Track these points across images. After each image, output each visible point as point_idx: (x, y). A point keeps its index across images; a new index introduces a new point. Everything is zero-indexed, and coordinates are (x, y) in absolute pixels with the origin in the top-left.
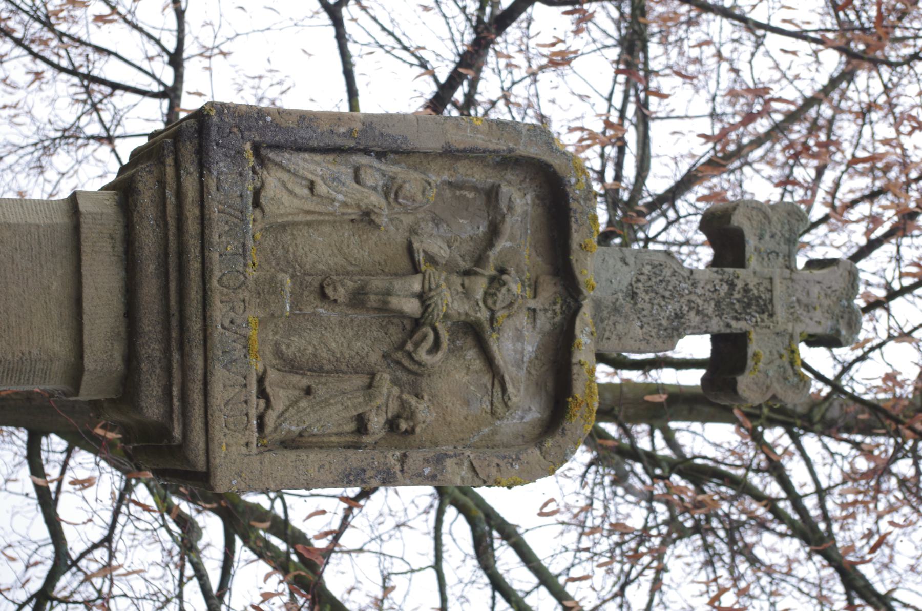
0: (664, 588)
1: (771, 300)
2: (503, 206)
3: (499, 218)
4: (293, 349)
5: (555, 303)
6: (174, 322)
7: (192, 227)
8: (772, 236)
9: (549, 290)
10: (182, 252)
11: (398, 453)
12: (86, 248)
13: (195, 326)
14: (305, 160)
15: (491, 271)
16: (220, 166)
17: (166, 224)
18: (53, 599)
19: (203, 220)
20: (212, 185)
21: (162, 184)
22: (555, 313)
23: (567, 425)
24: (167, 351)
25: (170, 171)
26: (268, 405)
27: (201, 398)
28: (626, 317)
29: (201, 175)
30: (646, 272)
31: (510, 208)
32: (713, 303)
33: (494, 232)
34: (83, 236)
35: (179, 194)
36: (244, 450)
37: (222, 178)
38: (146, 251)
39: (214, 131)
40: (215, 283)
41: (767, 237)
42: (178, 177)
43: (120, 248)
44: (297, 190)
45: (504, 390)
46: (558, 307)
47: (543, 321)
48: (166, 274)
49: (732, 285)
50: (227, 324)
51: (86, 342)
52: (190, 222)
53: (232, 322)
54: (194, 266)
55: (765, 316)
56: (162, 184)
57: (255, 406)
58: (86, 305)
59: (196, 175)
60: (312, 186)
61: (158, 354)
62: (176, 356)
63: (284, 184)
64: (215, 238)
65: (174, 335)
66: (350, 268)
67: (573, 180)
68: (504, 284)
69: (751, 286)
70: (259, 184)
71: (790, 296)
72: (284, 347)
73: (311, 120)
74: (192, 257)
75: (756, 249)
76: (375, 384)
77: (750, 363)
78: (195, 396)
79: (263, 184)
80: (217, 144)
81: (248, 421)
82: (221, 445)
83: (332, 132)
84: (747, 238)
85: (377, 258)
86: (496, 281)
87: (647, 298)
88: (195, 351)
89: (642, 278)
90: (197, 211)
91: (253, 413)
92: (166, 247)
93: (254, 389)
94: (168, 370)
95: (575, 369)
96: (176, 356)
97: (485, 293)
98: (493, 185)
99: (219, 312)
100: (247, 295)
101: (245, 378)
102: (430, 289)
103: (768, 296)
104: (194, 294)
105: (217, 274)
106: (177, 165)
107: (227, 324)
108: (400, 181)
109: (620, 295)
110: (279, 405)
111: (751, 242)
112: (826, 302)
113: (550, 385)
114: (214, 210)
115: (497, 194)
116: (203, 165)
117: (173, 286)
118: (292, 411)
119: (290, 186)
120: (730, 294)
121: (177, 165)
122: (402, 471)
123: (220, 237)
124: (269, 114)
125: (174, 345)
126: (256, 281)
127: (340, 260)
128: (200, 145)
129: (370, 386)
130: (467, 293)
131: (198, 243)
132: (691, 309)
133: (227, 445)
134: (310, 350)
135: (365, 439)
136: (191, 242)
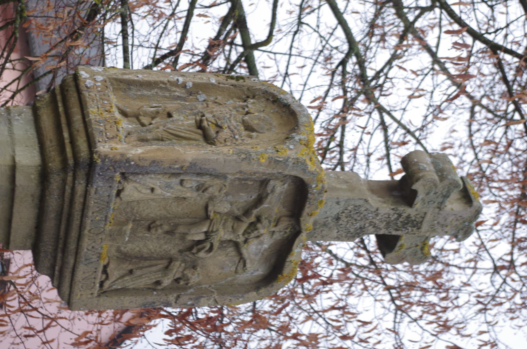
0: (395, 17)
1: (421, 222)
2: (269, 189)
3: (265, 195)
4: (127, 249)
5: (287, 229)
6: (61, 242)
7: (78, 206)
8: (435, 193)
9: (285, 224)
10: (70, 215)
11: (175, 295)
12: (17, 201)
13: (72, 246)
14: (152, 178)
15: (252, 219)
16: (99, 183)
17: (63, 200)
18: (38, 79)
19: (85, 205)
20: (93, 191)
21: (64, 181)
22: (286, 233)
23: (275, 284)
24: (56, 250)
25: (70, 179)
26: (107, 278)
27: (70, 275)
28: (330, 228)
29: (87, 186)
30: (349, 208)
31: (273, 191)
32: (385, 223)
33: (259, 201)
34: (16, 196)
35: (73, 189)
36: (90, 296)
37: (99, 189)
38: (51, 208)
39: (98, 169)
40: (86, 232)
41: (432, 194)
42: (74, 183)
43: (37, 201)
44: (144, 191)
45: (245, 265)
46: (288, 231)
47: (278, 236)
48: (60, 221)
49: (400, 215)
50: (90, 248)
51: (12, 238)
52: (77, 205)
53: (93, 247)
54: (76, 223)
55: (415, 229)
56: (64, 181)
57: (100, 276)
58: (14, 225)
59: (84, 185)
60: (152, 190)
61: (50, 250)
62: (60, 255)
63: (136, 188)
64: (90, 214)
65: (60, 246)
66: (169, 216)
67: (314, 186)
68: (257, 229)
69: (412, 216)
70: (121, 188)
71: (434, 220)
72: (122, 248)
73: (158, 162)
74: (75, 219)
75: (423, 200)
76: (170, 267)
77: (397, 248)
78: (67, 274)
79: (123, 189)
80: (99, 174)
81: (95, 285)
82: (77, 295)
83: (170, 168)
84: (418, 195)
85: (186, 211)
86: (253, 226)
87: (346, 220)
88: (70, 257)
89: (346, 211)
90: (82, 200)
91: (98, 282)
92: (62, 209)
93: (101, 269)
94: (55, 258)
95: (287, 264)
96: (60, 255)
97: (245, 231)
98: (266, 179)
99: (86, 243)
100: (104, 236)
101: (96, 269)
102: (212, 232)
103: (421, 220)
104: (74, 234)
105: (88, 228)
106: (74, 178)
107: (90, 248)
108: (207, 186)
109: (330, 219)
110: (112, 279)
111: (421, 196)
112: (455, 223)
113: (273, 260)
114: (92, 203)
115: (267, 184)
116: (89, 180)
117: (63, 227)
118: (120, 281)
119: (139, 189)
120: (397, 219)
121: (74, 178)
122: (176, 302)
123: (93, 213)
124: (133, 161)
125: (59, 250)
126: (110, 231)
127: (164, 212)
128: (89, 171)
129: (167, 268)
130: (234, 230)
131: (80, 213)
132: (370, 225)
133: (81, 295)
134: (138, 249)
135: (159, 287)
136: (76, 213)
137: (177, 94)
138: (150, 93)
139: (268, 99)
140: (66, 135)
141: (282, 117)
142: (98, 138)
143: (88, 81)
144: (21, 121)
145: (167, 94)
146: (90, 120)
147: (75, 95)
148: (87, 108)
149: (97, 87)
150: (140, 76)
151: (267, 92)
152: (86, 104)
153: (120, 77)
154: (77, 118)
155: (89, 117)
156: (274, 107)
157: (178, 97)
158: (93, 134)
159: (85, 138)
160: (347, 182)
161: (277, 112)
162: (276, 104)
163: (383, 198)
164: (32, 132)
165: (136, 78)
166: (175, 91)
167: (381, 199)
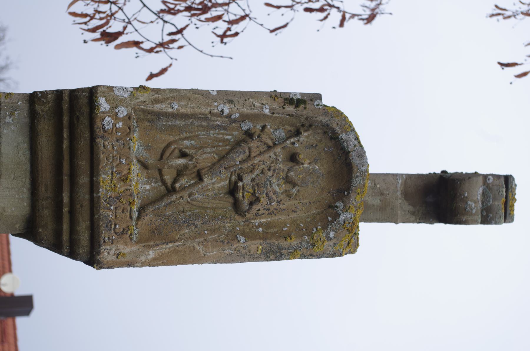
137: (217, 123)
138: (183, 123)
139: (325, 133)
140: (66, 198)
141: (335, 161)
142: (105, 235)
143: (108, 119)
144: (13, 127)
145: (205, 124)
146: (99, 197)
147: (87, 134)
148: (98, 175)
149: (117, 130)
150: (176, 105)
151: (328, 125)
152: (98, 165)
153: (150, 107)
154: (84, 180)
155: (99, 192)
156: (330, 144)
157: (218, 126)
158: (99, 226)
159: (88, 223)
160: (382, 194)
161: (332, 152)
162: (333, 141)
163: (414, 206)
164: (24, 155)
165: (170, 110)
166: (215, 121)
167: (411, 208)
